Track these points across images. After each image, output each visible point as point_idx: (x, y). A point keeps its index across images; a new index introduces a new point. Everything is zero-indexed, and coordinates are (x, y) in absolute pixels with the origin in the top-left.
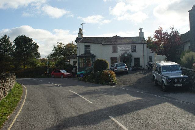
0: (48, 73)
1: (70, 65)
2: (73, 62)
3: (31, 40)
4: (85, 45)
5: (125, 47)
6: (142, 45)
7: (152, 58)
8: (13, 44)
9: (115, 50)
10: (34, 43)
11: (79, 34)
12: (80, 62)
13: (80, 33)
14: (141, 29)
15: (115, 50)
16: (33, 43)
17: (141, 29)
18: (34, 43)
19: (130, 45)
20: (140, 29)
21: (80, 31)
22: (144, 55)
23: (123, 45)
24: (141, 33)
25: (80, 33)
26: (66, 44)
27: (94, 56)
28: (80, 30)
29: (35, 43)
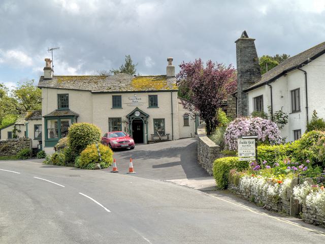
4: (58, 95)
9: (117, 103)
12: (49, 127)
15: (117, 103)
21: (47, 64)
22: (172, 114)
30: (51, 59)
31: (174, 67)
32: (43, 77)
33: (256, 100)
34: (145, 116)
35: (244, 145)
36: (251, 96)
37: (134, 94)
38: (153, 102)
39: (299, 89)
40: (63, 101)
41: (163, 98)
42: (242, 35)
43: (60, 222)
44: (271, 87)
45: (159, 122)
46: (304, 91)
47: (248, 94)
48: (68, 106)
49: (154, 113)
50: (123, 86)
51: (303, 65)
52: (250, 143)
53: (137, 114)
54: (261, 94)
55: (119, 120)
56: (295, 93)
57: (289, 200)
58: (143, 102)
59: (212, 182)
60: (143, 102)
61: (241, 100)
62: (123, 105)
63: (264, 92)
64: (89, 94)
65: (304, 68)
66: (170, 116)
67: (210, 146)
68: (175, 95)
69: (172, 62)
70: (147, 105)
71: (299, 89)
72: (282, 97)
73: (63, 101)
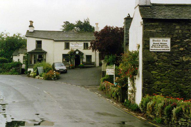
5: (77, 44)
13: (31, 26)
15: (67, 46)
19: (83, 43)
25: (31, 26)
40: (39, 43)
48: (41, 47)
64: (52, 41)
73: (39, 43)
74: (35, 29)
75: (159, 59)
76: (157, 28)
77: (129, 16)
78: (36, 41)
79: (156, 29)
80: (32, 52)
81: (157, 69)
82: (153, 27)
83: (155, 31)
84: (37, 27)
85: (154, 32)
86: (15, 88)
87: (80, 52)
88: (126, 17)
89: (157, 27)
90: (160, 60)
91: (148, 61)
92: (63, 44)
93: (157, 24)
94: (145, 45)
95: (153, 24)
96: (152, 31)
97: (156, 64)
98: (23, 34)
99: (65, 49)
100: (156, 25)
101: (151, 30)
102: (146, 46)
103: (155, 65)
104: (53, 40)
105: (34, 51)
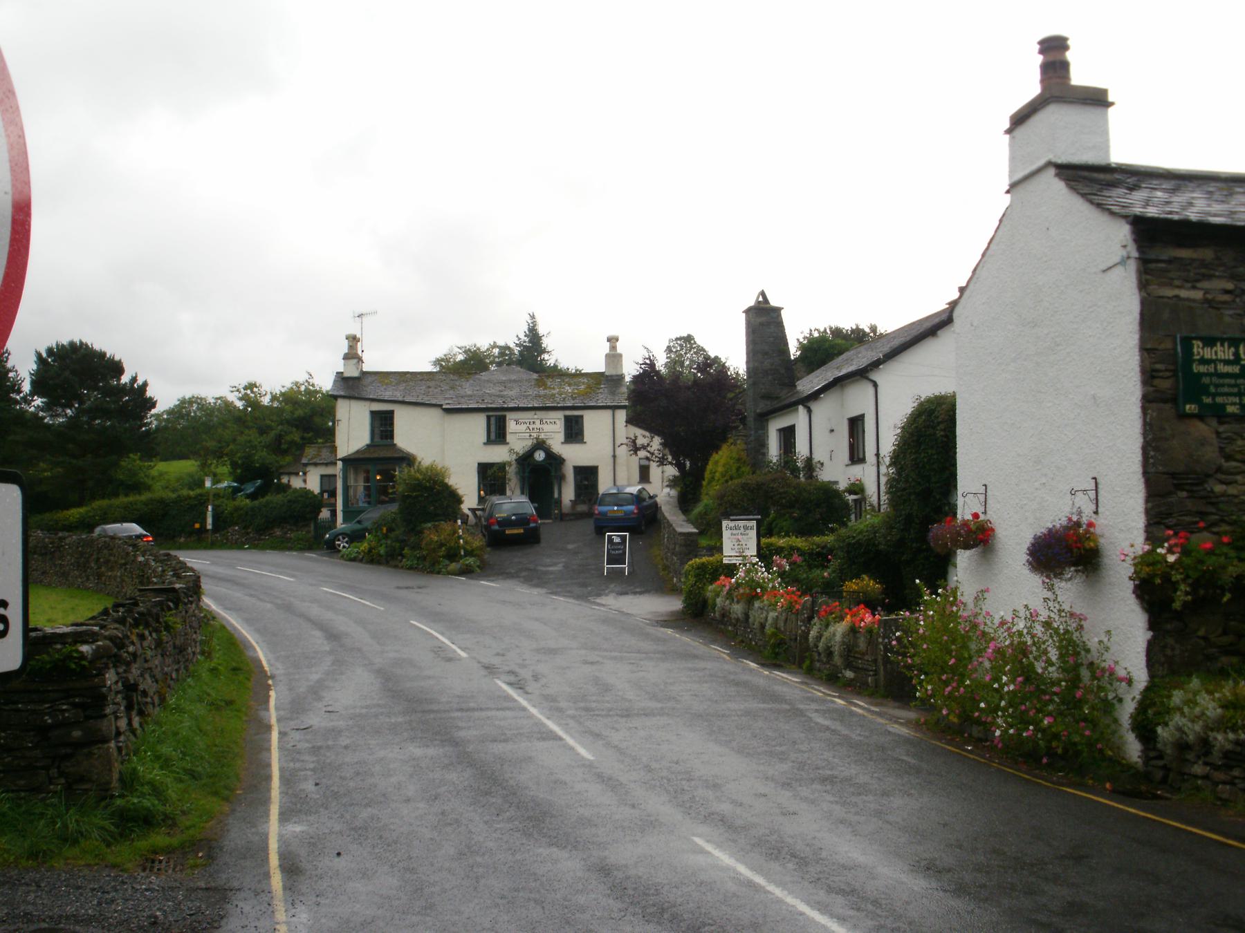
0: (209, 527)
1: (306, 493)
2: (318, 480)
3: (116, 368)
4: (373, 413)
5: (538, 422)
6: (608, 413)
7: (28, 214)
8: (26, 387)
9: (497, 434)
10: (134, 379)
11: (347, 357)
12: (351, 482)
13: (352, 356)
14: (613, 340)
15: (497, 434)
16: (125, 379)
17: (613, 340)
18: (134, 379)
19: (560, 415)
20: (609, 340)
21: (351, 347)
22: (614, 456)
23: (530, 415)
24: (614, 357)
25: (352, 356)
26: (277, 390)
27: (407, 459)
28: (353, 340)
29: (140, 381)
30: (358, 336)
31: (621, 356)
32: (342, 373)
33: (782, 433)
34: (555, 461)
35: (735, 532)
36: (774, 427)
37: (533, 412)
38: (574, 432)
39: (861, 417)
40: (383, 424)
41: (597, 425)
42: (758, 297)
43: (508, 672)
44: (810, 411)
45: (587, 475)
46: (874, 421)
47: (767, 421)
48: (392, 437)
49: (574, 455)
50: (513, 396)
51: (871, 370)
52: (746, 528)
53: (540, 456)
54: (793, 423)
55: (502, 467)
56: (856, 424)
57: (796, 639)
58: (553, 430)
59: (675, 604)
60: (553, 430)
61: (752, 432)
62: (509, 438)
63: (799, 419)
64: (436, 413)
65: (875, 376)
66: (612, 460)
67: (679, 530)
68: (622, 416)
69: (618, 344)
70: (561, 437)
71: (861, 417)
72: (832, 431)
73: (383, 424)
74: (366, 368)
75: (1229, 458)
76: (1209, 277)
77: (766, 300)
78: (373, 413)
79: (1206, 284)
80: (357, 456)
81: (1222, 521)
82: (1196, 274)
83: (1198, 295)
84: (374, 361)
85: (1194, 301)
86: (501, 712)
87: (550, 455)
88: (752, 303)
89: (1204, 272)
90: (1234, 464)
91: (1173, 475)
92: (477, 426)
93: (1207, 254)
94: (1153, 377)
95: (1185, 253)
96: (1184, 294)
97: (1212, 491)
98: (325, 383)
99: (489, 442)
100: (1203, 264)
101: (1176, 292)
102: (1156, 382)
103: (1211, 500)
104: (440, 406)
105: (367, 456)
